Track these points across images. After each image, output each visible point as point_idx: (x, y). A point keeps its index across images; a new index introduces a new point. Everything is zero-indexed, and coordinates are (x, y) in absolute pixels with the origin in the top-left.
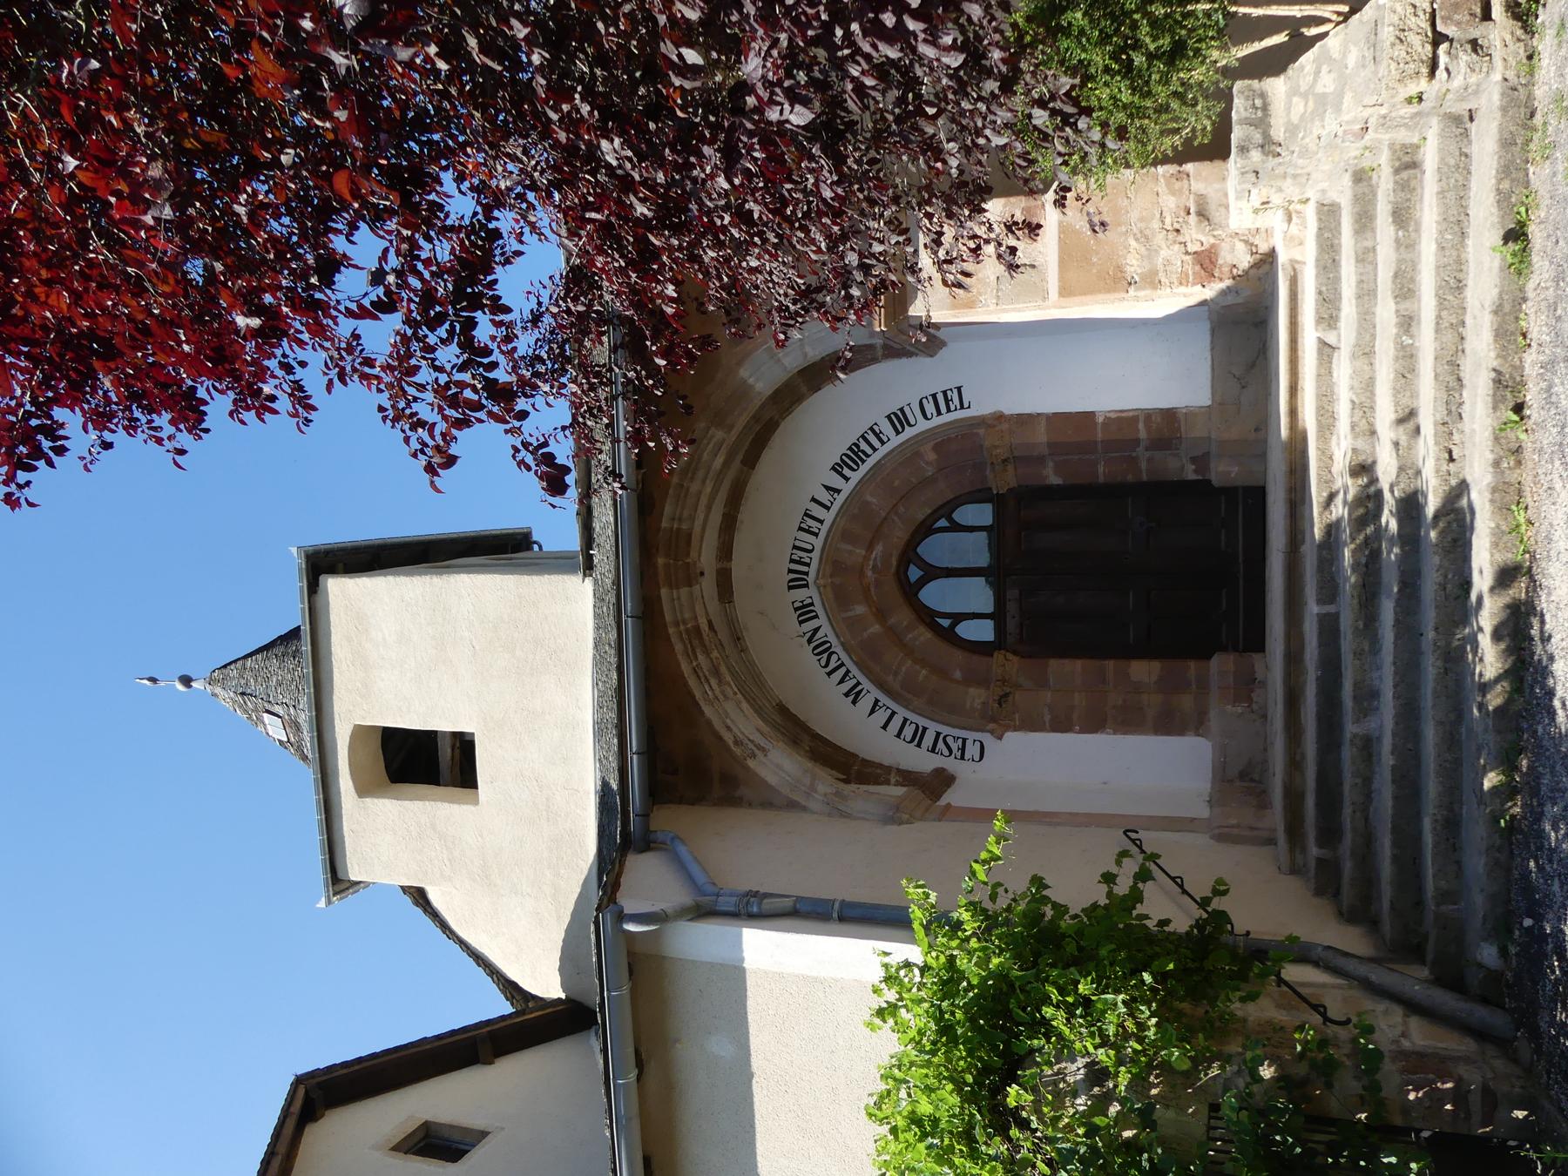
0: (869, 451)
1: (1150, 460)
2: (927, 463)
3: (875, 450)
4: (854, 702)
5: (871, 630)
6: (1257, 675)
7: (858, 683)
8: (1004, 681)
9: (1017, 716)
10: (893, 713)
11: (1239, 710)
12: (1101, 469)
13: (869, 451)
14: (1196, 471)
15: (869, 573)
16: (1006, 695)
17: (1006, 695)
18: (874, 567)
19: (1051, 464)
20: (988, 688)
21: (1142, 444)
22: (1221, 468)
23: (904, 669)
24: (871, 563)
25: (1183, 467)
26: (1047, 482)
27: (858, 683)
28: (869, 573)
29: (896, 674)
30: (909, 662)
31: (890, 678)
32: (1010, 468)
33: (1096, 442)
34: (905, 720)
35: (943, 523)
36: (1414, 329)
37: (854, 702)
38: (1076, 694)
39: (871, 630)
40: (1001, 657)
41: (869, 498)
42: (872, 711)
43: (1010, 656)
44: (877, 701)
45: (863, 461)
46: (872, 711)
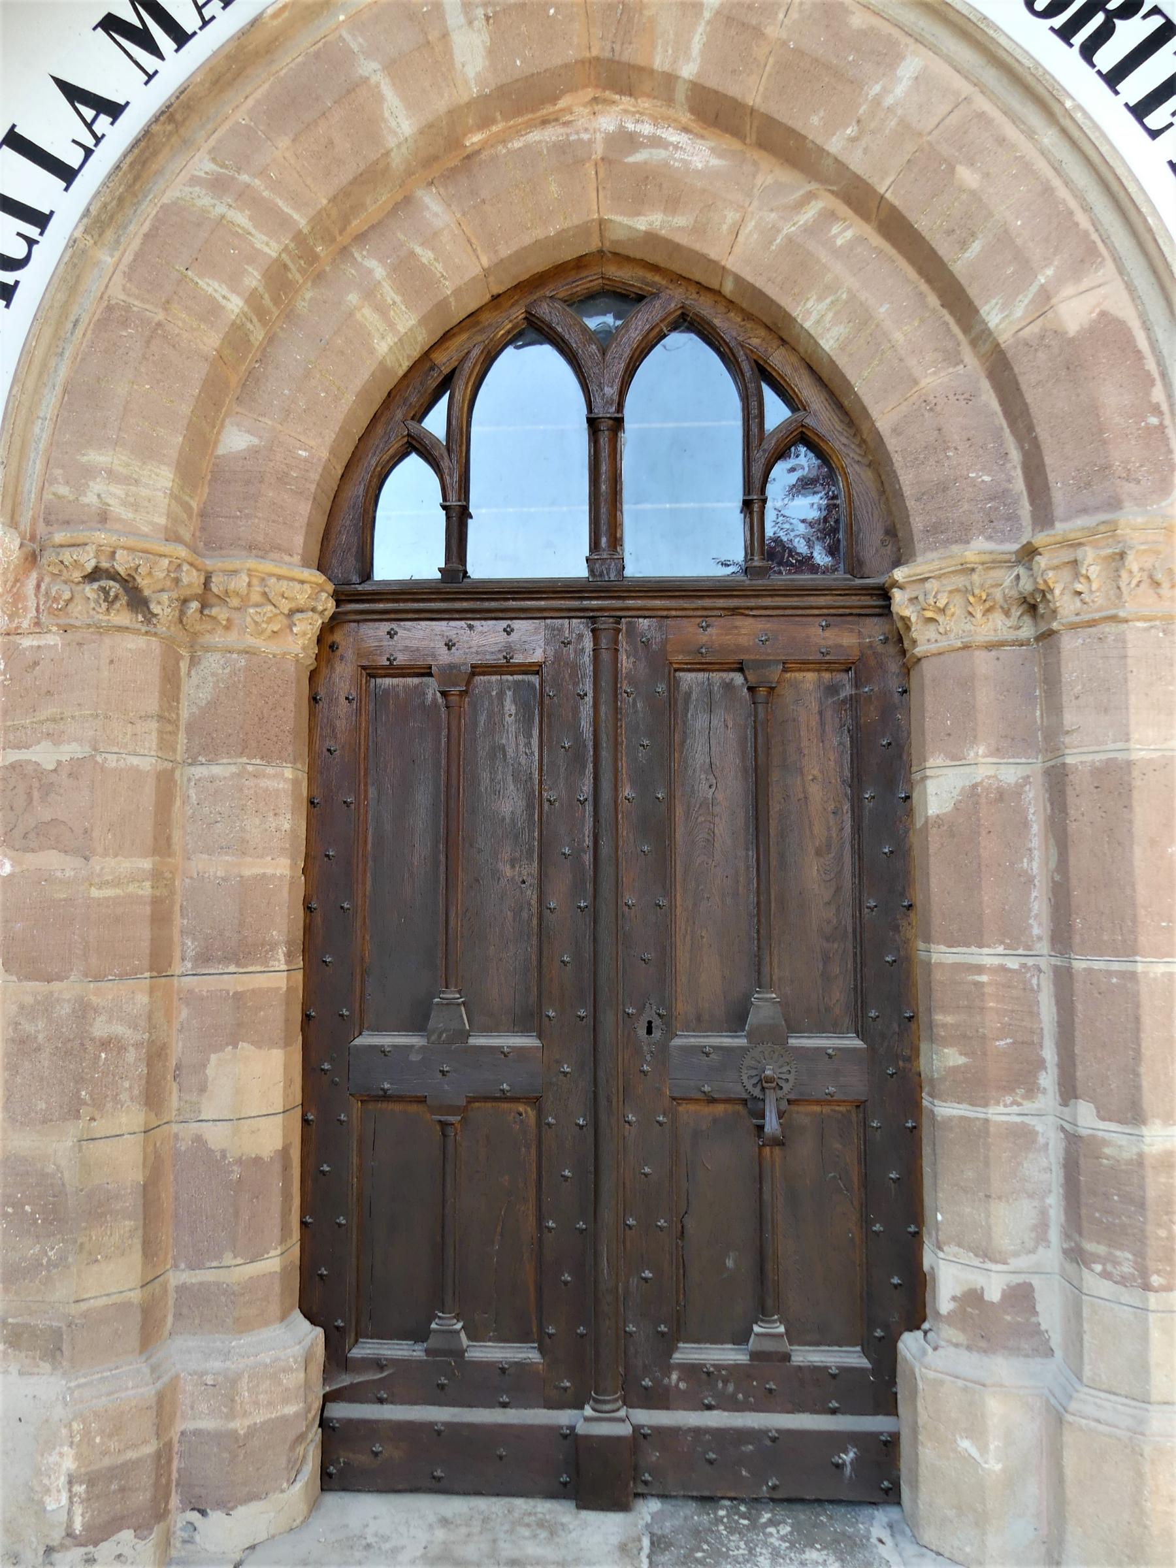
0: (1109, 55)
1: (1023, 1137)
2: (1045, 297)
3: (1114, 78)
4: (111, 24)
5: (391, 99)
6: (215, 1516)
7: (181, 37)
8: (206, 597)
9: (53, 639)
10: (67, 174)
11: (57, 1502)
12: (989, 956)
13: (1109, 55)
14: (973, 1298)
15: (607, 122)
16: (138, 601)
17: (138, 601)
18: (628, 141)
19: (1010, 774)
20: (172, 537)
21: (1112, 1134)
22: (995, 1407)
23: (241, 219)
24: (646, 129)
25: (987, 1253)
26: (935, 761)
27: (181, 37)
28: (607, 122)
29: (218, 185)
30: (269, 246)
31: (202, 165)
32: (998, 626)
33: (1129, 949)
34: (40, 220)
35: (776, 413)
36: (169, 103)
37: (111, 24)
38: (146, 864)
39: (391, 99)
40: (302, 596)
41: (911, 65)
42: (74, 94)
43: (308, 627)
44: (114, 110)
45: (1066, 33)
46: (74, 94)
